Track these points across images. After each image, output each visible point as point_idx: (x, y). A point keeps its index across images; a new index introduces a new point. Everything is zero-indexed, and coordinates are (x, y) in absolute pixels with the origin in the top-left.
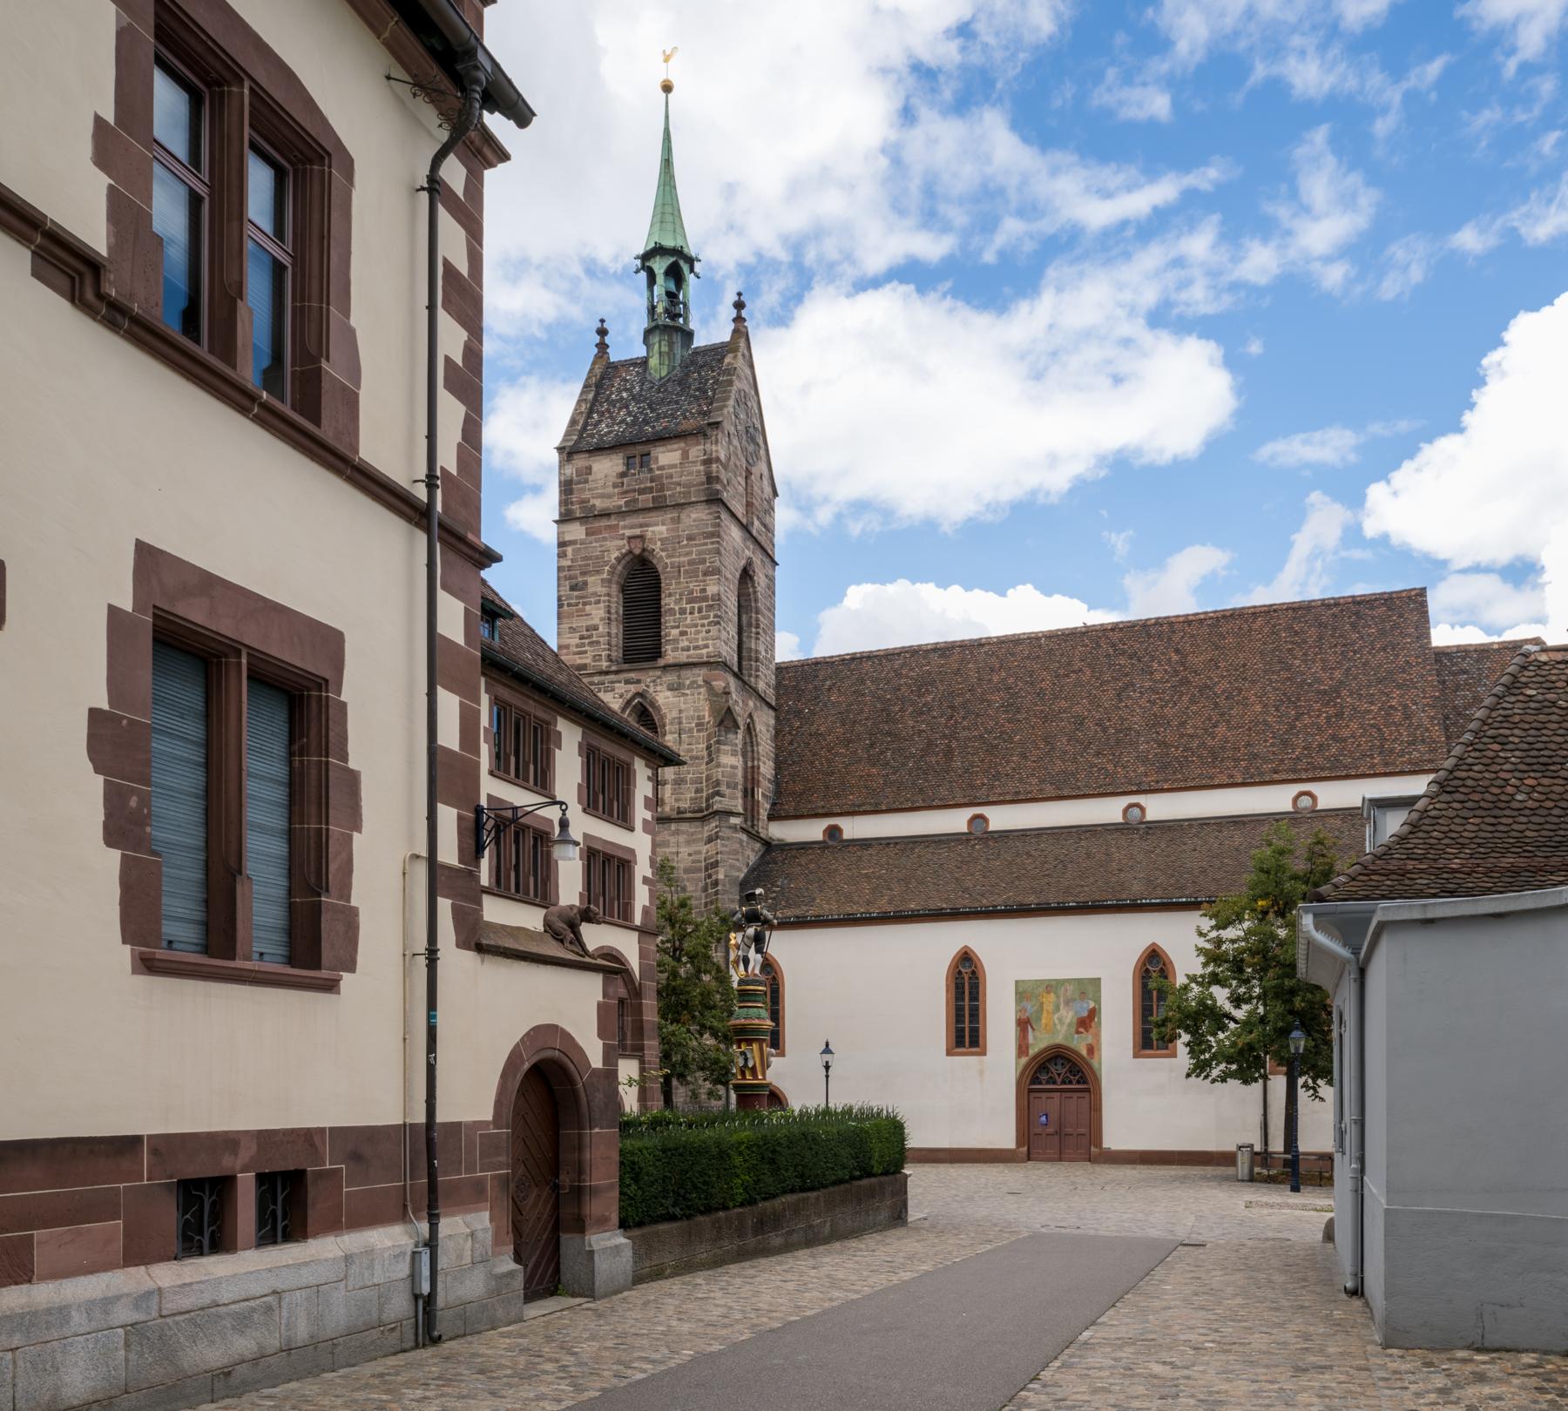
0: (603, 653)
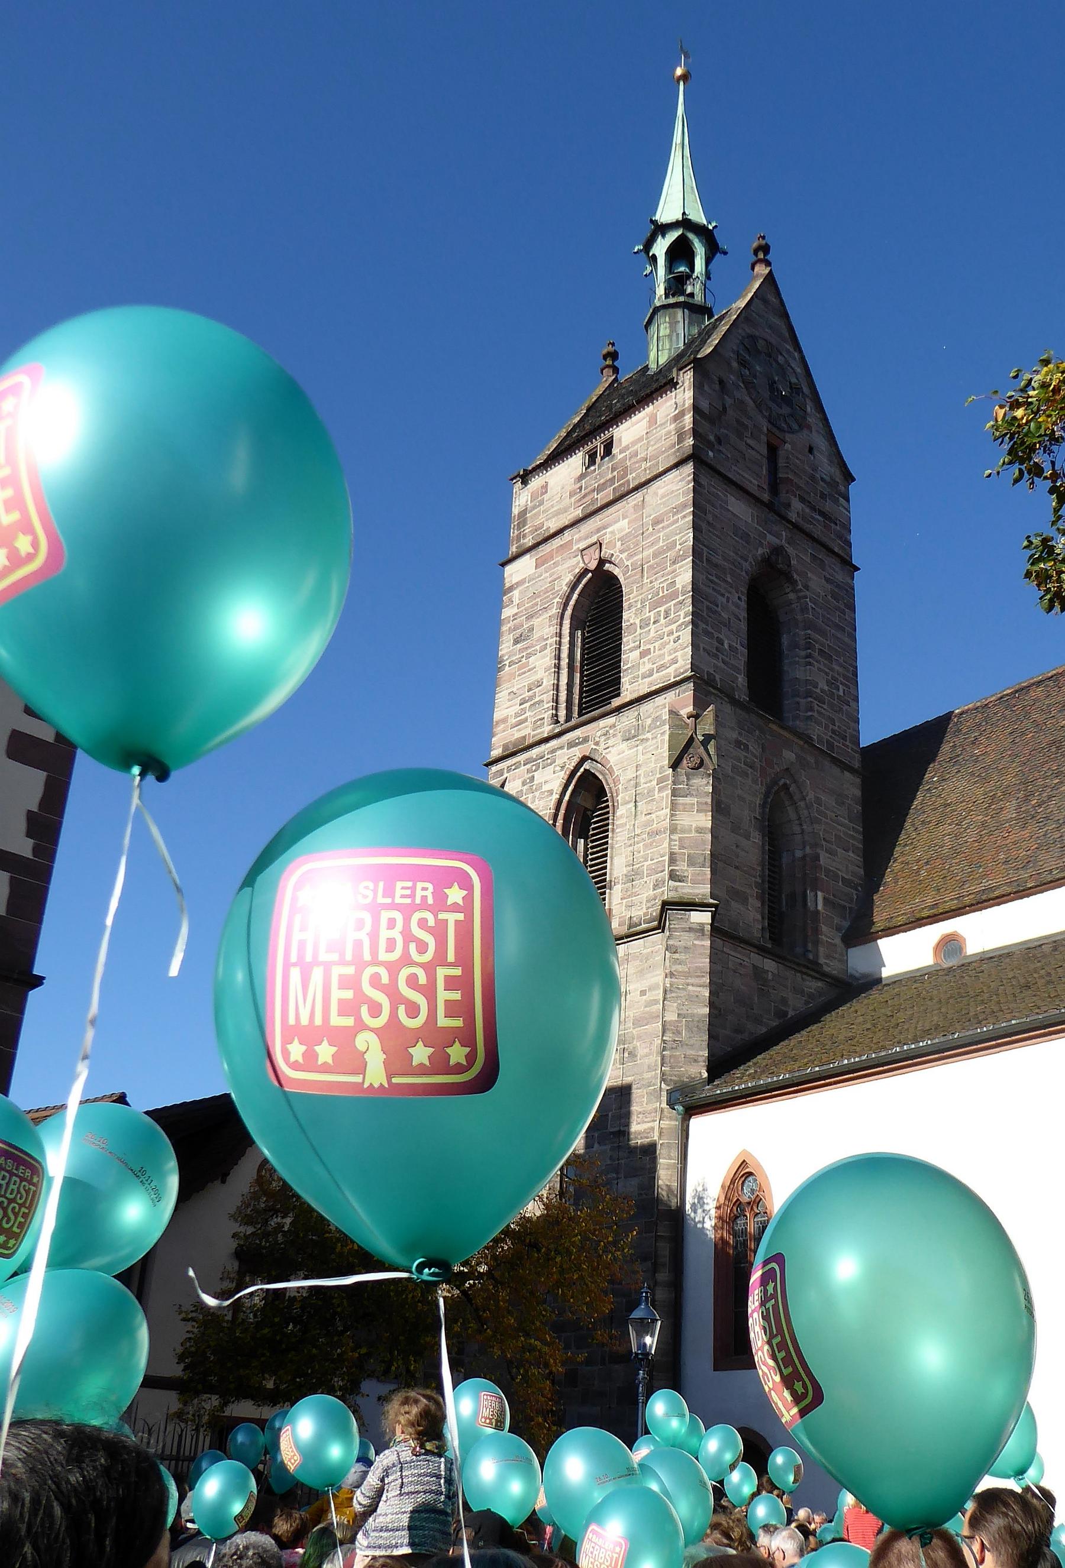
0: (546, 715)
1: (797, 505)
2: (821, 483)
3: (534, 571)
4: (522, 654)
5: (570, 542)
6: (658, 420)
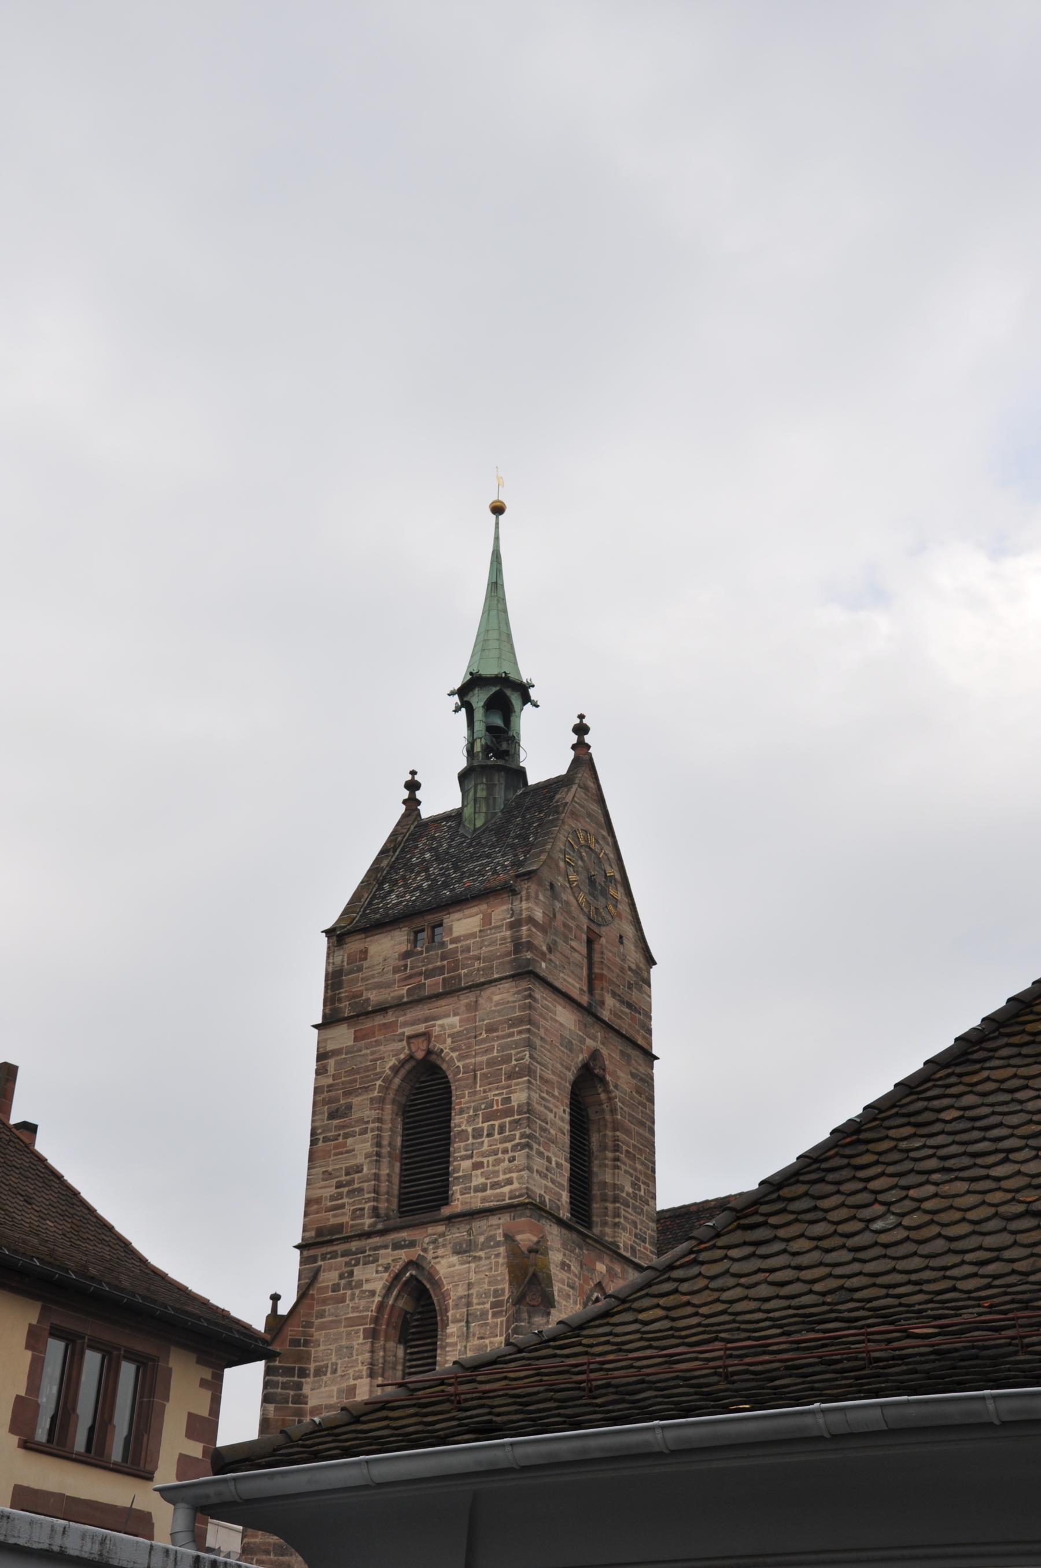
0: (367, 1206)
1: (610, 1001)
2: (629, 973)
3: (351, 1043)
4: (338, 1132)
6: (493, 921)
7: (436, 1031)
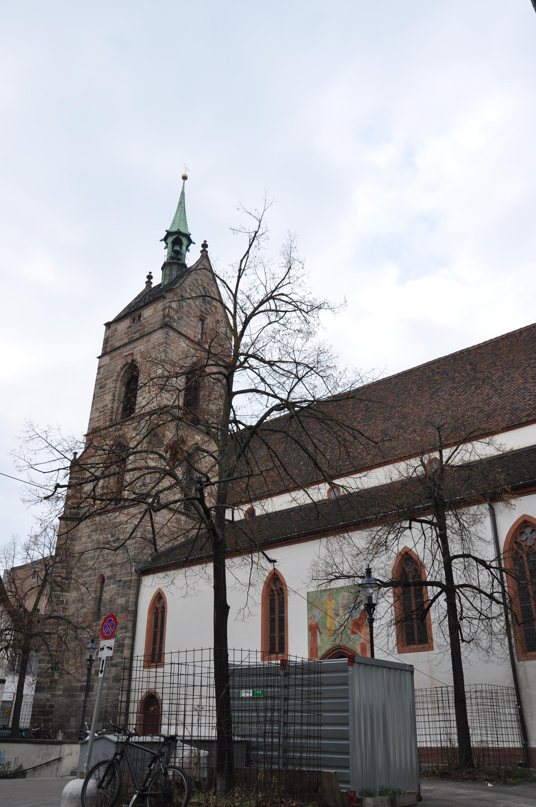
5: (122, 352)
7: (135, 352)
